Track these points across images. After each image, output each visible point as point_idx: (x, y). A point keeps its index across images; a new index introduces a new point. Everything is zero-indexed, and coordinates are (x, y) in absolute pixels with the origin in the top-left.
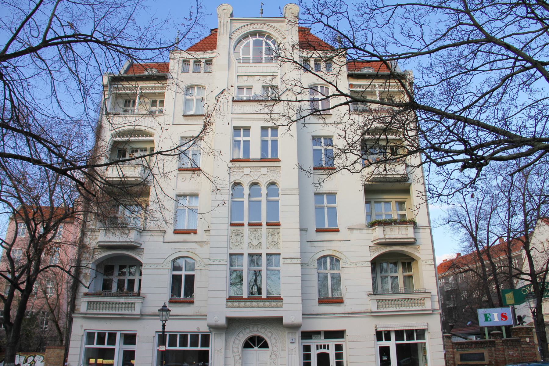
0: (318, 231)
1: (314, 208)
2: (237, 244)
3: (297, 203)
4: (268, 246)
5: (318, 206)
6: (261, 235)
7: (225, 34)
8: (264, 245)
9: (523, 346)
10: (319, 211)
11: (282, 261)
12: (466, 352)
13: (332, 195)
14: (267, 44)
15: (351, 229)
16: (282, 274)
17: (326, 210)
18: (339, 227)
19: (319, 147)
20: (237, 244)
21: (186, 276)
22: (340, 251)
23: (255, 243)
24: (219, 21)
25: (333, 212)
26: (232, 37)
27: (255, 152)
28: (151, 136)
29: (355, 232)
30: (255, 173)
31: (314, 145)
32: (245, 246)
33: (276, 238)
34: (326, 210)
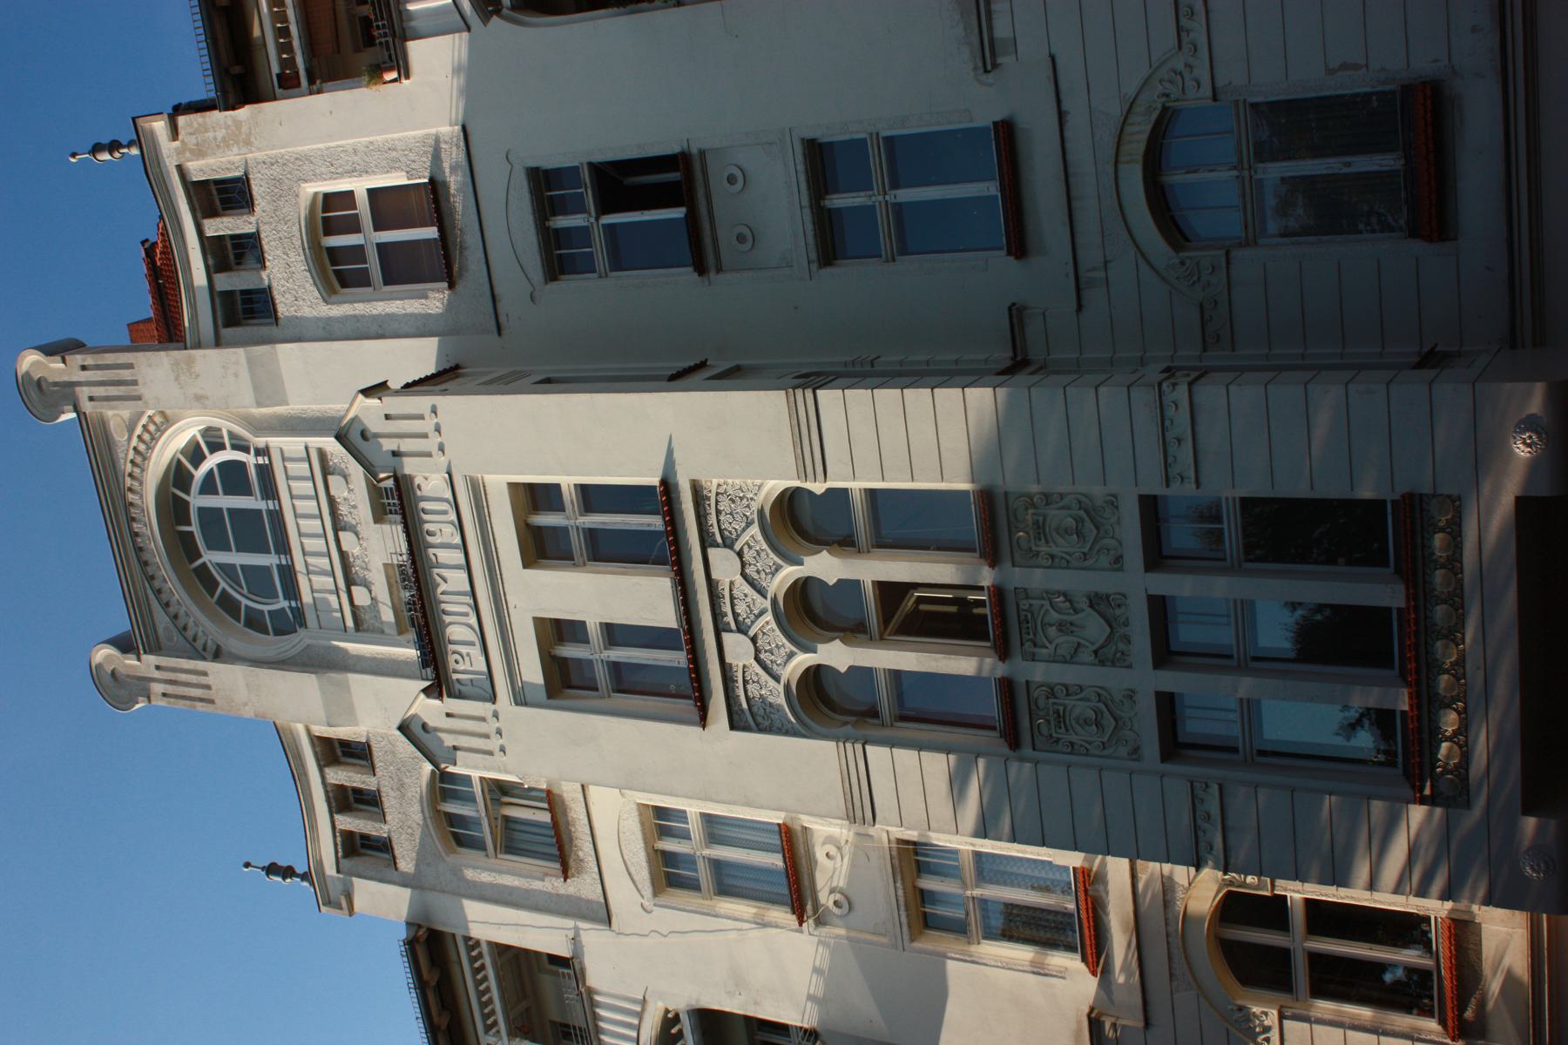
0: (1018, 246)
1: (907, 264)
2: (1109, 723)
3: (859, 397)
4: (1104, 561)
5: (885, 242)
6: (1048, 595)
7: (202, 680)
8: (1103, 582)
9: (1385, 162)
10: (913, 233)
11: (1185, 490)
12: (873, 162)
13: (823, 163)
14: (208, 486)
15: (989, 55)
16: (1256, 487)
17: (905, 195)
18: (984, 118)
19: (598, 239)
20: (1109, 723)
21: (1284, 955)
22: (1116, 110)
23: (1094, 628)
24: (163, 703)
25: (909, 155)
26: (211, 646)
27: (644, 598)
28: (676, 1019)
29: (1001, 29)
30: (741, 608)
31: (585, 266)
32: (1114, 679)
33: (1056, 516)
34: (905, 195)
